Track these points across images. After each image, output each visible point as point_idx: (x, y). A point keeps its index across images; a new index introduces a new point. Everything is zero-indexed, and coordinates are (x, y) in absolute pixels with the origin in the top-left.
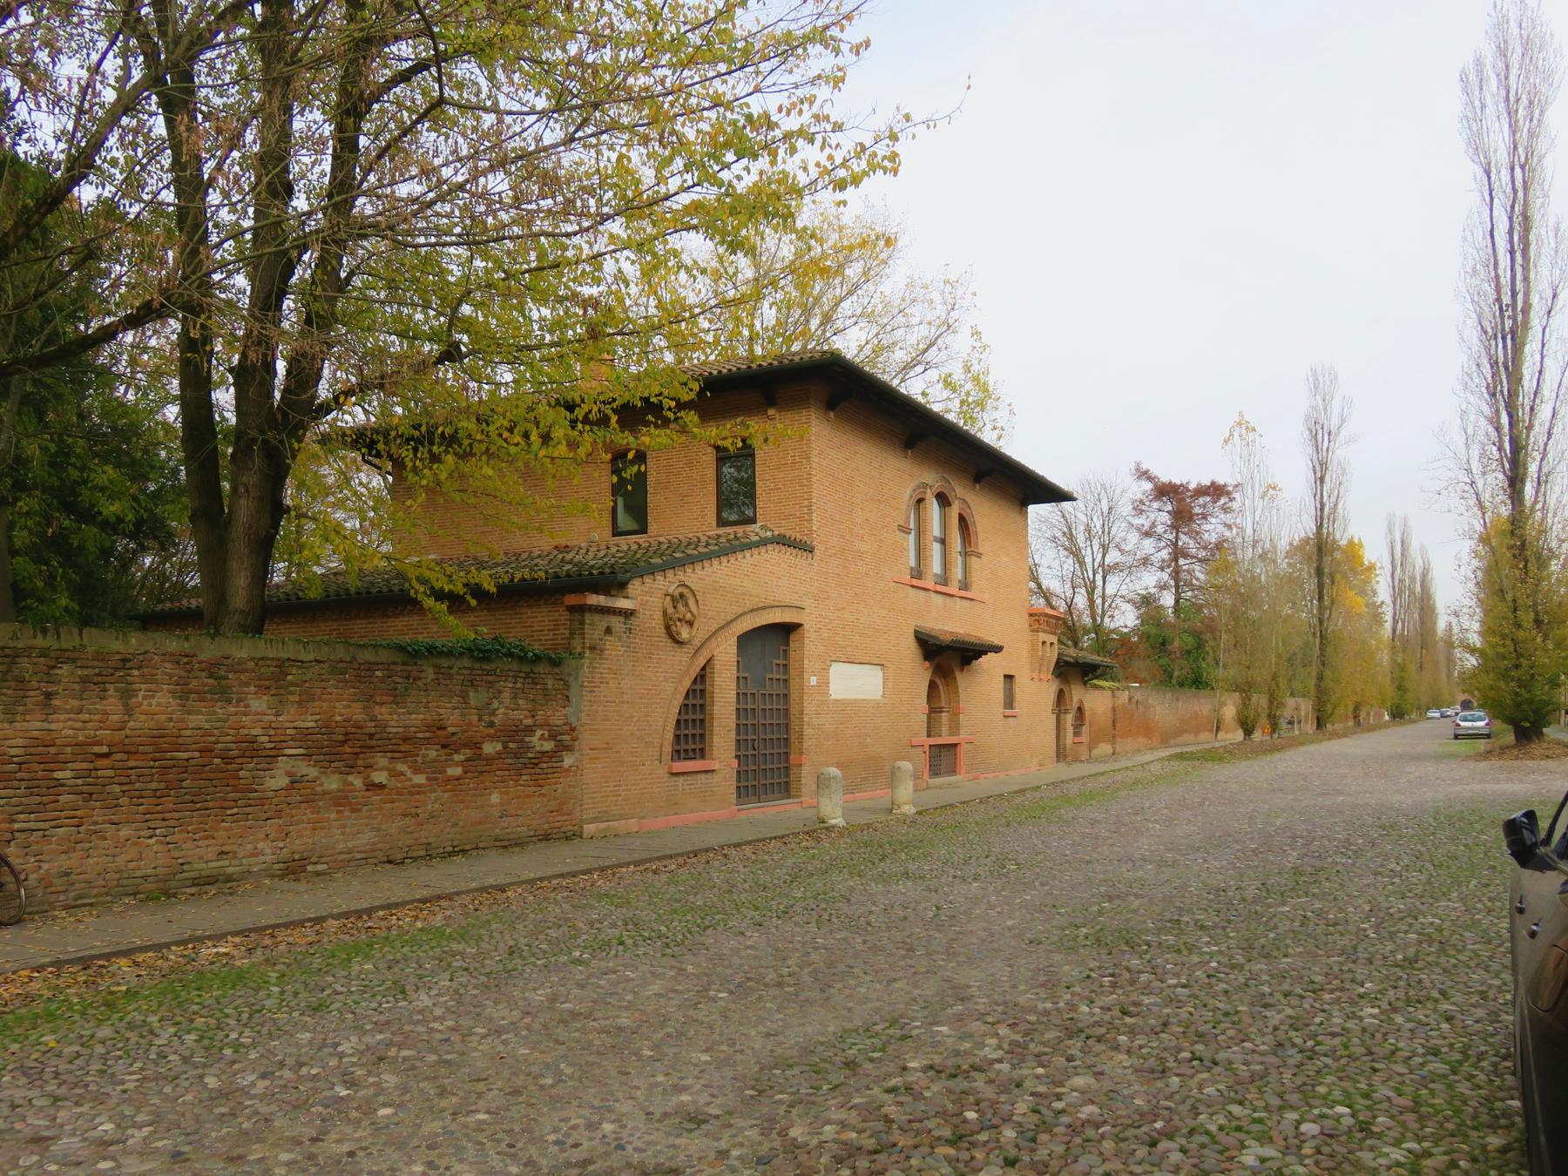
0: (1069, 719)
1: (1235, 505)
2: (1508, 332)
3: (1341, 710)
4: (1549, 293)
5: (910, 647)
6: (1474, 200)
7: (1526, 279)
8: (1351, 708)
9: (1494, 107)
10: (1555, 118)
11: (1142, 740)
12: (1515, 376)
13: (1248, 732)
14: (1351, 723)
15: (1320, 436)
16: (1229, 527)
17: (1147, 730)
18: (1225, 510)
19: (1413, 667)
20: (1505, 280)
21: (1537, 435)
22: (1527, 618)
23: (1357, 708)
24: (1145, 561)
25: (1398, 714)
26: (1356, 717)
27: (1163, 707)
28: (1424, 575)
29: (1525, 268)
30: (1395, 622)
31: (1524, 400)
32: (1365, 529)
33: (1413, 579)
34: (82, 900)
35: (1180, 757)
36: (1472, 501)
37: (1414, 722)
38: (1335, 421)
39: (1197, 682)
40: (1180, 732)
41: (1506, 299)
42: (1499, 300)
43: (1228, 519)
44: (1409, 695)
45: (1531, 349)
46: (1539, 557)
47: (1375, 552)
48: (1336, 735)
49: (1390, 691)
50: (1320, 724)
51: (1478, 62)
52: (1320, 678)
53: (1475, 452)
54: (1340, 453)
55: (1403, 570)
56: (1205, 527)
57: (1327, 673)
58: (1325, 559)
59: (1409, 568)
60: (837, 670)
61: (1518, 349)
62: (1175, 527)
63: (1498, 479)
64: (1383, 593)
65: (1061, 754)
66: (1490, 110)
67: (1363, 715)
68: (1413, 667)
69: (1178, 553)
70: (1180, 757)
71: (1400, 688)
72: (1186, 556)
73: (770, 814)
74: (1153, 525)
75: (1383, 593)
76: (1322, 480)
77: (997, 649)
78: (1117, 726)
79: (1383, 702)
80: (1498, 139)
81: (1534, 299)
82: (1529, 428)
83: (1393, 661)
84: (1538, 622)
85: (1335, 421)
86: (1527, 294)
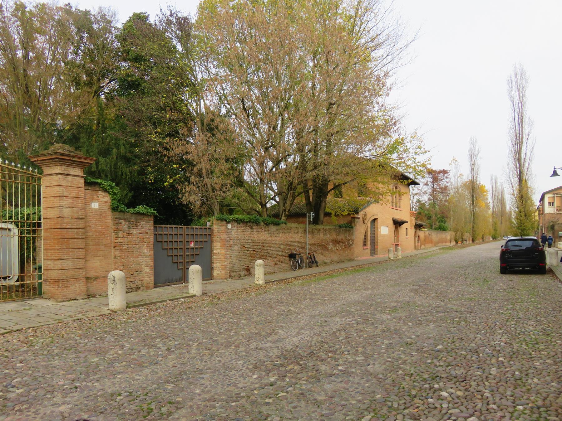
0: (417, 238)
1: (449, 176)
2: (518, 142)
3: (478, 237)
4: (527, 134)
5: (392, 222)
6: (511, 111)
7: (522, 131)
8: (481, 236)
9: (515, 89)
10: (527, 93)
11: (430, 245)
12: (520, 154)
13: (457, 243)
14: (481, 241)
15: (472, 156)
16: (448, 182)
17: (431, 242)
18: (447, 178)
19: (499, 223)
20: (518, 131)
21: (525, 169)
22: (523, 214)
23: (483, 236)
24: (425, 193)
25: (495, 238)
26: (482, 239)
27: (435, 236)
28: (502, 192)
29: (522, 129)
30: (493, 208)
31: (522, 161)
32: (484, 181)
33: (498, 194)
34: (51, 297)
35: (443, 248)
36: (511, 185)
37: (499, 240)
38: (476, 153)
39: (442, 229)
40: (438, 242)
41: (518, 136)
42: (516, 135)
43: (448, 180)
44: (498, 232)
45: (524, 148)
46: (526, 199)
47: (488, 187)
48: (477, 244)
49: (492, 231)
50: (473, 241)
51: (511, 77)
52: (473, 227)
53: (511, 173)
54: (478, 161)
55: (496, 192)
56: (442, 182)
57: (475, 226)
58: (474, 189)
59: (497, 191)
60: (382, 228)
61: (520, 148)
62: (433, 182)
63: (517, 180)
64: (490, 200)
65: (415, 248)
66: (514, 89)
67: (485, 238)
68: (499, 223)
69: (434, 190)
70: (443, 248)
71: (495, 230)
72: (436, 191)
73: (374, 257)
74: (427, 182)
75: (490, 200)
76: (473, 169)
77: (407, 222)
78: (427, 240)
79: (490, 234)
80: (516, 96)
81: (524, 136)
82: (523, 167)
83: (493, 221)
84: (525, 215)
85: (476, 153)
86: (522, 135)
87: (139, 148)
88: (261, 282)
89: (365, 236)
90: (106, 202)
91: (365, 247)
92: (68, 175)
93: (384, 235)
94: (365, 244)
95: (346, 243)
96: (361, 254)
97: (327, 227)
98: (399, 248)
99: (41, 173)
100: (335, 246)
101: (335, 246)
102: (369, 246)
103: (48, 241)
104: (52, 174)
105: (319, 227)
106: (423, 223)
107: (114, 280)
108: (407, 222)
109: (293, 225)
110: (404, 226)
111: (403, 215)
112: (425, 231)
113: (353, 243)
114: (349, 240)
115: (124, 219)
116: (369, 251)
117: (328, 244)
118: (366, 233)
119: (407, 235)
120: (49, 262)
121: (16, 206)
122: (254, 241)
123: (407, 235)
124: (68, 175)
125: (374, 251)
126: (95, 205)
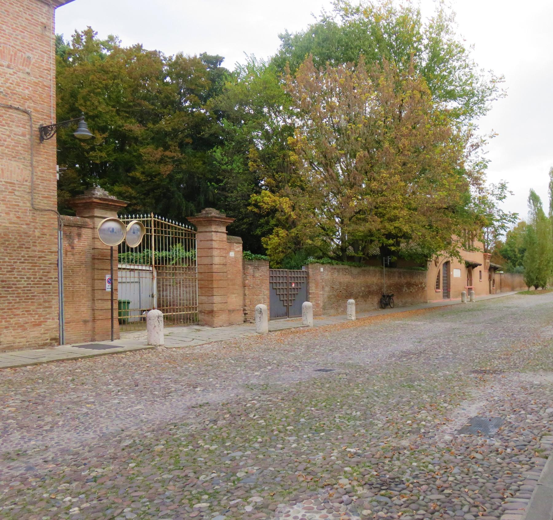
0: (492, 282)
5: (528, 194)
60: (455, 270)
73: (447, 301)
77: (480, 265)
78: (502, 286)
87: (153, 155)
88: (353, 318)
89: (438, 279)
90: (238, 251)
91: (438, 290)
92: (217, 232)
93: (457, 278)
94: (438, 287)
95: (420, 286)
96: (435, 297)
97: (401, 270)
98: (473, 291)
99: (195, 230)
100: (409, 289)
101: (409, 289)
102: (441, 290)
103: (202, 282)
104: (206, 232)
105: (394, 270)
106: (498, 266)
107: (261, 311)
108: (480, 265)
109: (372, 268)
110: (476, 270)
111: (477, 257)
112: (501, 274)
113: (425, 286)
114: (422, 283)
115: (250, 265)
116: (441, 294)
117: (402, 286)
118: (439, 273)
119: (480, 278)
120: (203, 298)
121: (159, 250)
122: (340, 283)
123: (480, 278)
124: (217, 232)
125: (447, 294)
126: (232, 254)
